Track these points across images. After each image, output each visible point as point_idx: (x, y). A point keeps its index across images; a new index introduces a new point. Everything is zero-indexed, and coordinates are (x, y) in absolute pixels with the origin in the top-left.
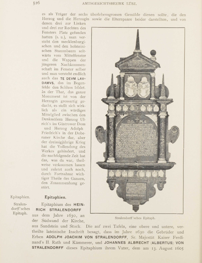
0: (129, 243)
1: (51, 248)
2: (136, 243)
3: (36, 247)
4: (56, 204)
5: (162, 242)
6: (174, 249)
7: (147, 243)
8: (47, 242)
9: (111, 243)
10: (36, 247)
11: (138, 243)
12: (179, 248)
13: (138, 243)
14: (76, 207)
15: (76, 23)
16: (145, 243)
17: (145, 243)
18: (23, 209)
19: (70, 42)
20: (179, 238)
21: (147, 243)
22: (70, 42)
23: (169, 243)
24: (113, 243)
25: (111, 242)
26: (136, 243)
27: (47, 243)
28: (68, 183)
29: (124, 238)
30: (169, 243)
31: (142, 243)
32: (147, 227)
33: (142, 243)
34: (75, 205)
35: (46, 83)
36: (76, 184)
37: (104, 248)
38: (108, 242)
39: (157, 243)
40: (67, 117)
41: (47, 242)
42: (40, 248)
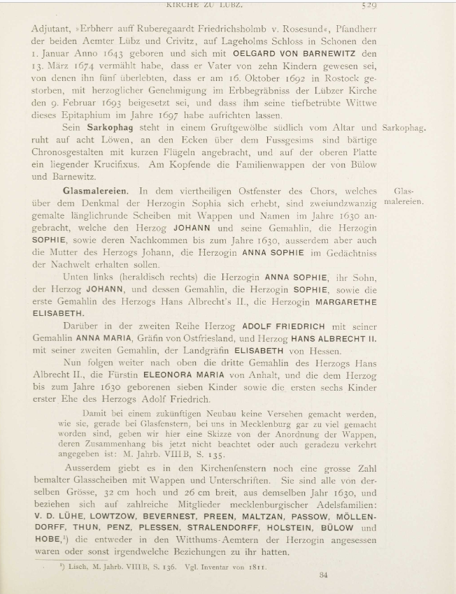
0: (320, 339)
1: (231, 527)
2: (335, 339)
3: (197, 527)
4: (95, 113)
5: (166, 515)
6: (343, 415)
7: (361, 339)
8: (76, 373)
9: (101, 290)
10: (197, 527)
11: (342, 339)
12: (295, 77)
13: (342, 339)
14: (247, 522)
15: (187, 351)
16: (357, 340)
17: (357, 340)
18: (157, 278)
19: (252, 506)
20: (310, 241)
21: (361, 339)
22: (252, 506)
23: (330, 529)
24: (300, 339)
25: (101, 287)
26: (335, 339)
27: (76, 376)
28: (119, 164)
29: (58, 529)
30: (330, 529)
31: (350, 339)
32: (162, 30)
33: (350, 339)
34: (38, 540)
35: (247, 252)
36: (179, 326)
37: (296, 469)
38: (94, 289)
39: (329, 340)
40: (165, 295)
41: (76, 373)
42: (204, 528)
